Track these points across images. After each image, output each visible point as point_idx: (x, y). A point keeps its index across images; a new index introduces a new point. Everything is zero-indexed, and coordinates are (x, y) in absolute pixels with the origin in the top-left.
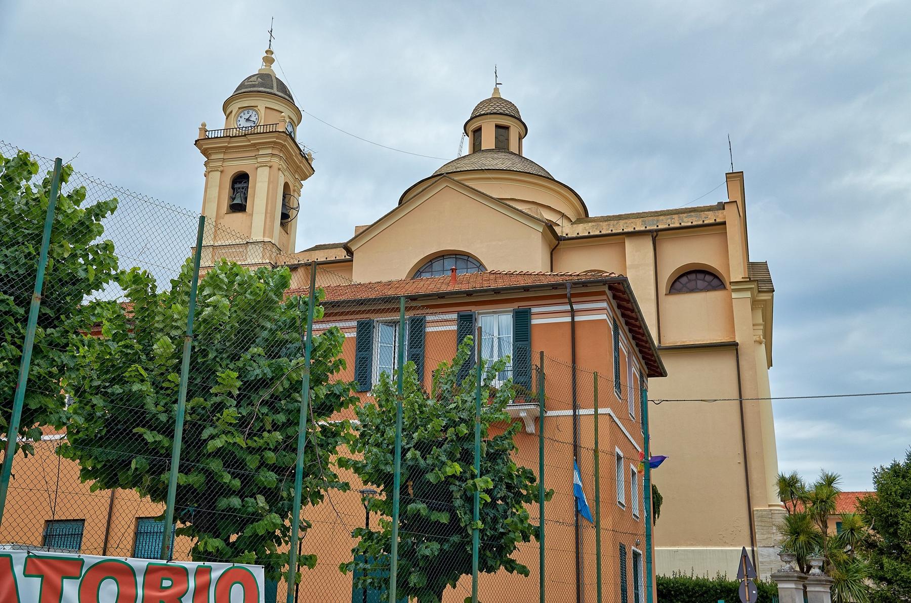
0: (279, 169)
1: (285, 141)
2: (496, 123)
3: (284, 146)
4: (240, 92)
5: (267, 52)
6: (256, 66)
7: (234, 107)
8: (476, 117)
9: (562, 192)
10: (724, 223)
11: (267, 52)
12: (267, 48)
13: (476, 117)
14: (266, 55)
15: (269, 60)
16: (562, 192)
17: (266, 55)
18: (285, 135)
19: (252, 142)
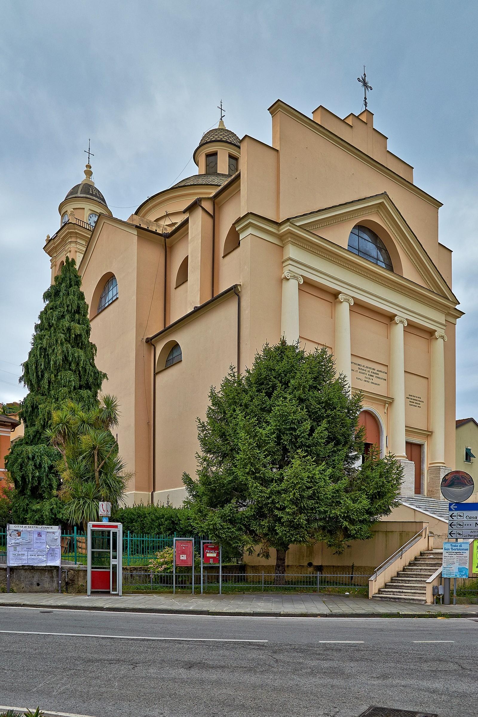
0: (76, 252)
1: (75, 229)
2: (205, 153)
3: (76, 233)
4: (69, 197)
5: (87, 166)
6: (81, 178)
7: (69, 208)
8: (207, 143)
9: (159, 201)
10: (84, 209)
11: (87, 166)
12: (87, 164)
13: (207, 143)
14: (86, 169)
15: (89, 173)
16: (159, 201)
17: (86, 169)
18: (72, 225)
19: (76, 231)
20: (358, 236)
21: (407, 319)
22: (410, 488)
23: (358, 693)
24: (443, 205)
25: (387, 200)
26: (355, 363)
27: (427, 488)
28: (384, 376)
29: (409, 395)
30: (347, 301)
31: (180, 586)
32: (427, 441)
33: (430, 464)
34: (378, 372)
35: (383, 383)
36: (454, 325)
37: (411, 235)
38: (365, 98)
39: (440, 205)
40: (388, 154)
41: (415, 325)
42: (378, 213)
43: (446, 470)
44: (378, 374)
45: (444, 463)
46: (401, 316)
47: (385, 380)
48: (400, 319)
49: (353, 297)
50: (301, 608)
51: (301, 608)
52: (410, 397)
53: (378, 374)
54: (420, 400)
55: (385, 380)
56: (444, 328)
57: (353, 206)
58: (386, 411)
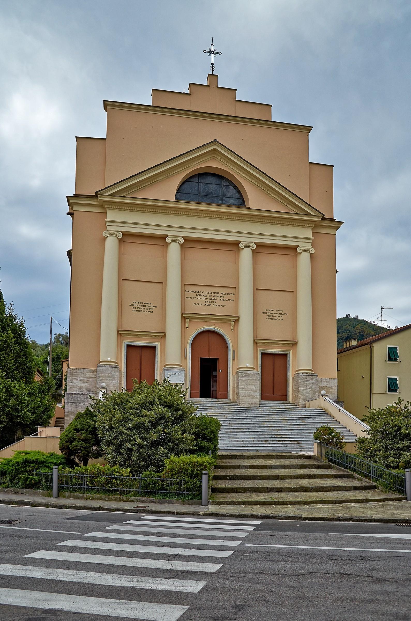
20: (198, 182)
21: (255, 243)
22: (253, 396)
23: (394, 601)
24: (312, 127)
25: (219, 146)
26: (192, 292)
27: (292, 394)
28: (231, 297)
29: (267, 310)
30: (176, 241)
31: (164, 490)
32: (291, 351)
33: (296, 371)
34: (222, 295)
35: (230, 305)
36: (335, 235)
37: (252, 168)
38: (213, 64)
39: (309, 128)
40: (237, 103)
41: (263, 245)
42: (214, 158)
43: (308, 377)
44: (223, 297)
45: (312, 371)
46: (244, 240)
47: (233, 300)
48: (245, 244)
49: (182, 237)
50: (95, 504)
51: (95, 504)
52: (267, 312)
53: (223, 297)
54: (283, 313)
55: (233, 300)
56: (311, 241)
57: (181, 159)
58: (232, 328)
